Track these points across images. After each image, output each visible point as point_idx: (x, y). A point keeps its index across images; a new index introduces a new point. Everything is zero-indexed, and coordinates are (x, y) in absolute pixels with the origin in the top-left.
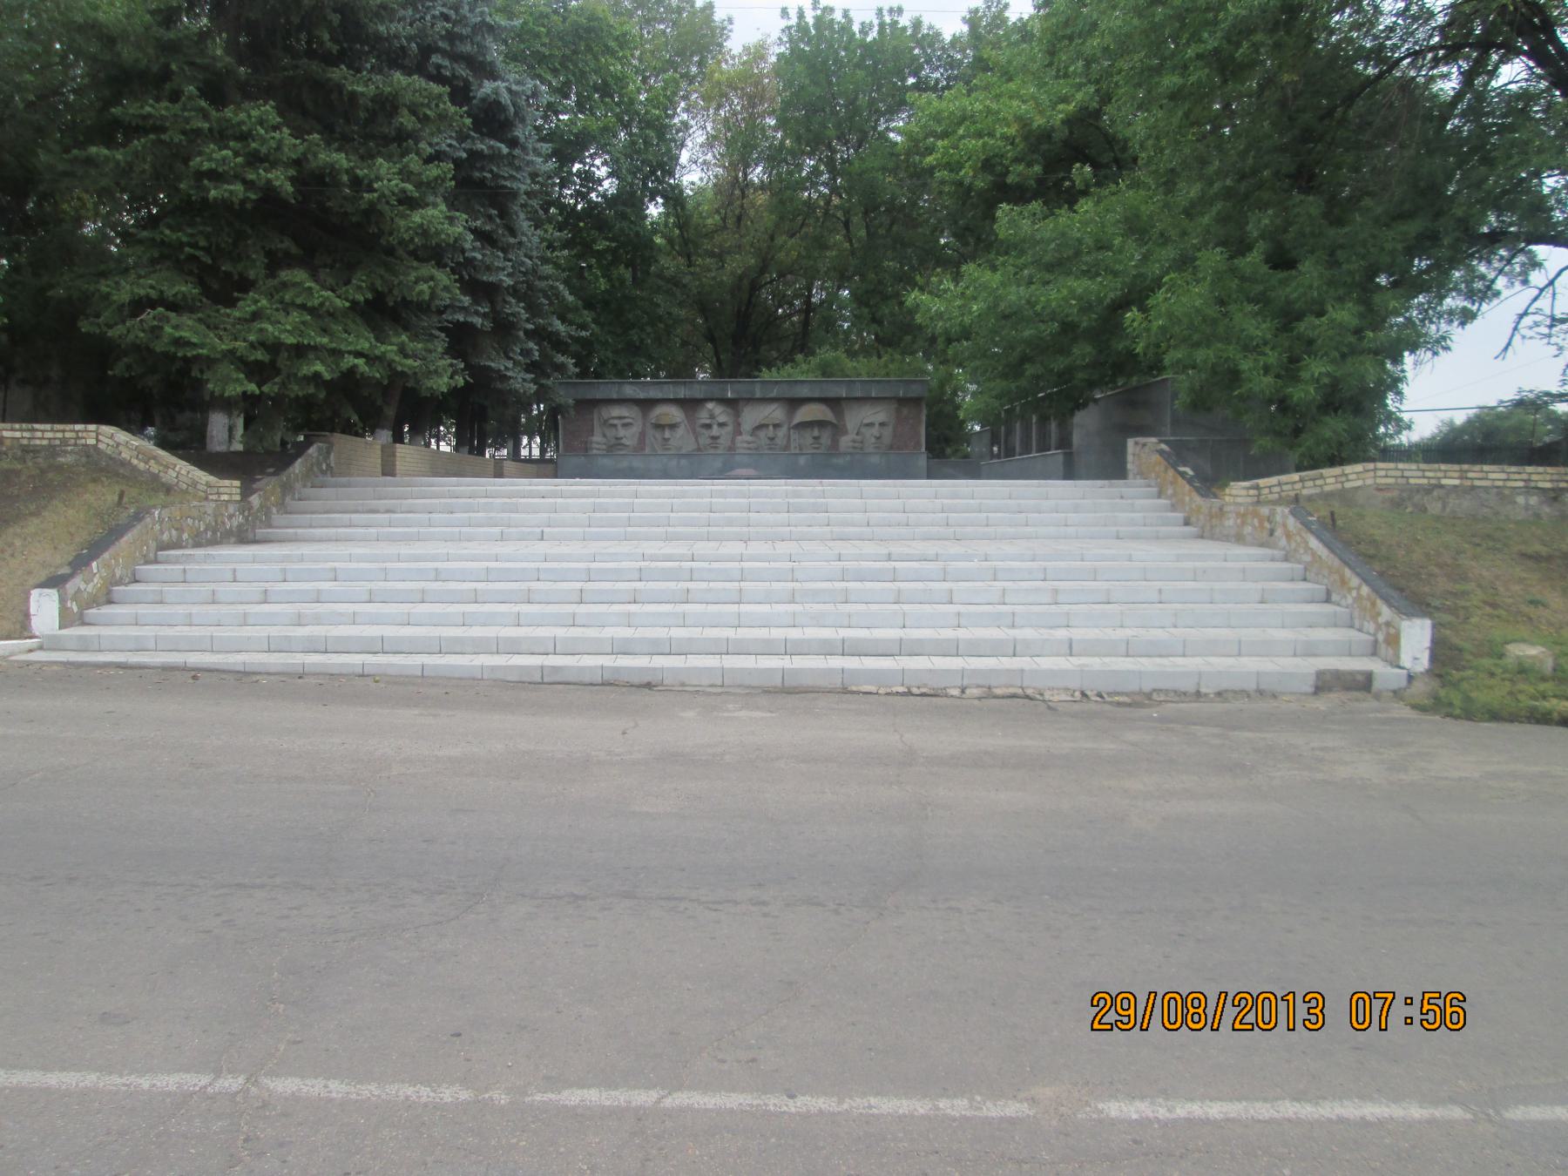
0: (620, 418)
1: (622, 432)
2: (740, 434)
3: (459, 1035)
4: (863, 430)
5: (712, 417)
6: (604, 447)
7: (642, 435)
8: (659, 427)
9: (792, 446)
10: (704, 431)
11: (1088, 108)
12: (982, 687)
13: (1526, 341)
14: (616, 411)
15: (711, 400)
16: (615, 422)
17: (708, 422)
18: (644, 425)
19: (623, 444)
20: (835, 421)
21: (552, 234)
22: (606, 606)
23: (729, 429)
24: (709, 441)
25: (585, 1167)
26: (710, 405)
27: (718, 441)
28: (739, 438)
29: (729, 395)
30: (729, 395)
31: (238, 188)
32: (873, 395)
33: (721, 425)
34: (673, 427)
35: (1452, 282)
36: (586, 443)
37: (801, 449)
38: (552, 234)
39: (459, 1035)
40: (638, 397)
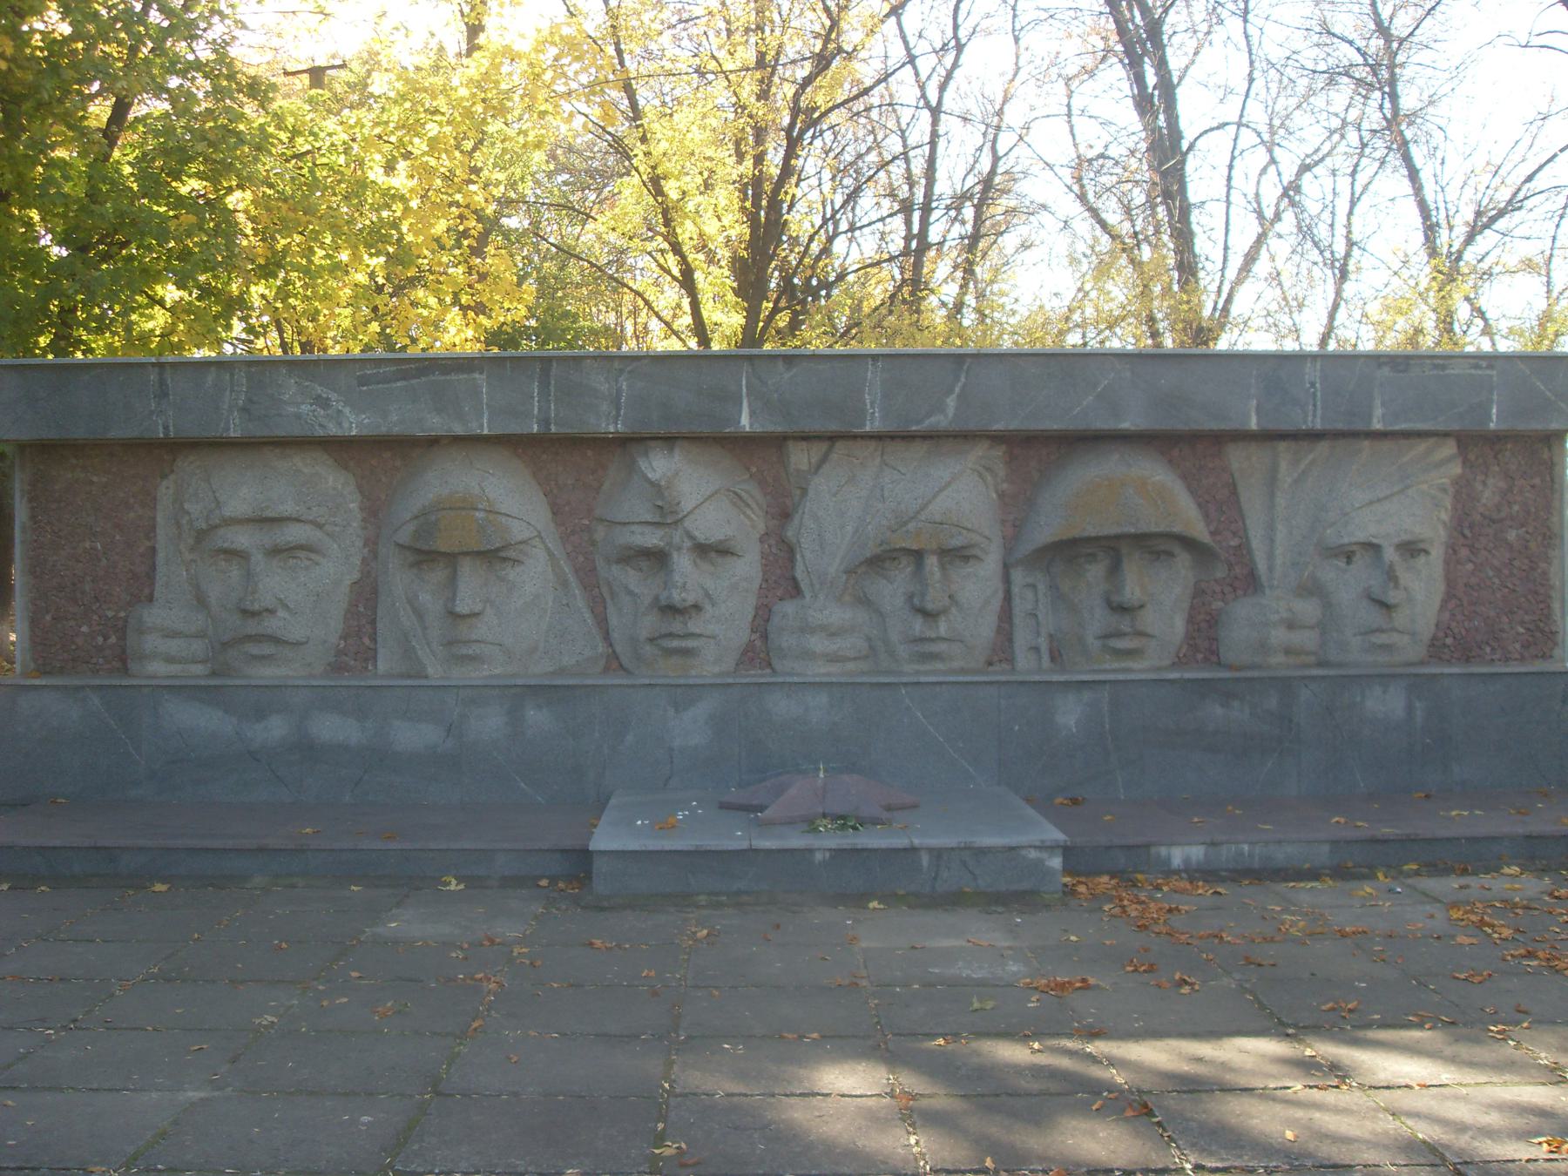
0: (263, 521)
1: (274, 583)
3: (384, 14)
4: (1329, 573)
5: (667, 515)
6: (198, 647)
9: (1022, 638)
10: (630, 577)
13: (992, 98)
15: (669, 440)
16: (242, 539)
17: (652, 539)
18: (372, 543)
19: (275, 640)
20: (1199, 530)
23: (747, 567)
24: (649, 624)
25: (370, 201)
26: (658, 465)
27: (694, 626)
28: (789, 607)
30: (745, 421)
31: (950, 291)
32: (1377, 425)
33: (707, 551)
34: (495, 556)
36: (122, 632)
37: (1055, 656)
39: (384, 14)
40: (333, 430)
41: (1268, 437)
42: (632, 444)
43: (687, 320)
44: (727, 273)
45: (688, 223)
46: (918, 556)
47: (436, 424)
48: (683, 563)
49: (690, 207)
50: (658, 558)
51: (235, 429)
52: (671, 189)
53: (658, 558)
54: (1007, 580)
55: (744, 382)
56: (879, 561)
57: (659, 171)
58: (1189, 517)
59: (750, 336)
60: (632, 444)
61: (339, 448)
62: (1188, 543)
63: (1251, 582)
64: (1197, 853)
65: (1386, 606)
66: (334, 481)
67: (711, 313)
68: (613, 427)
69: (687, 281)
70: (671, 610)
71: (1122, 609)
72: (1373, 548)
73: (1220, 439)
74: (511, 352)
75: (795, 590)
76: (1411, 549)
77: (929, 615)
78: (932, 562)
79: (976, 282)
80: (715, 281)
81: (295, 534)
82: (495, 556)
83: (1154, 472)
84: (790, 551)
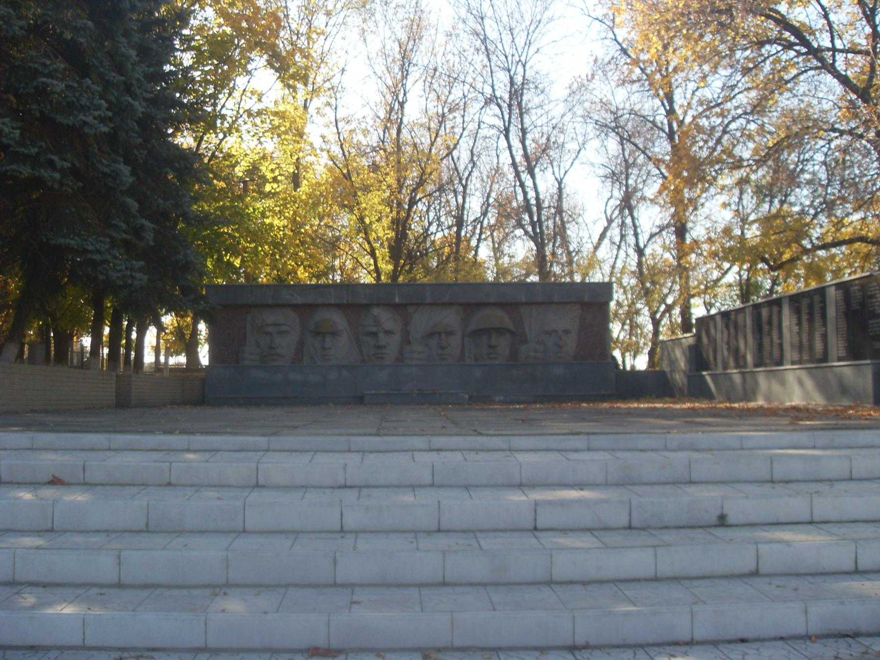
2: (409, 343)
5: (377, 323)
7: (301, 344)
8: (318, 333)
11: (527, 114)
12: (646, 652)
14: (270, 317)
15: (378, 305)
16: (270, 329)
17: (374, 329)
19: (278, 355)
20: (511, 327)
21: (657, 43)
22: (665, 569)
23: (397, 337)
26: (375, 311)
29: (397, 300)
30: (397, 300)
32: (556, 300)
33: (388, 333)
34: (334, 334)
35: (736, 245)
37: (476, 360)
38: (657, 43)
40: (295, 302)
41: (528, 304)
42: (368, 306)
43: (372, 268)
44: (387, 250)
45: (373, 233)
46: (440, 334)
47: (320, 300)
48: (381, 336)
49: (374, 226)
50: (375, 334)
51: (270, 302)
52: (367, 221)
53: (375, 334)
54: (463, 340)
55: (808, 423)
56: (431, 335)
57: (363, 214)
58: (508, 323)
59: (394, 275)
60: (368, 306)
61: (295, 307)
62: (509, 331)
63: (525, 341)
64: (502, 398)
65: (560, 347)
66: (292, 315)
67: (382, 265)
68: (365, 302)
69: (373, 254)
70: (379, 347)
71: (491, 347)
72: (556, 331)
73: (518, 304)
74: (323, 281)
75: (409, 343)
76: (566, 332)
77: (443, 348)
78: (443, 336)
79: (526, 233)
80: (382, 252)
81: (284, 328)
82: (334, 334)
83: (499, 313)
84: (408, 333)
